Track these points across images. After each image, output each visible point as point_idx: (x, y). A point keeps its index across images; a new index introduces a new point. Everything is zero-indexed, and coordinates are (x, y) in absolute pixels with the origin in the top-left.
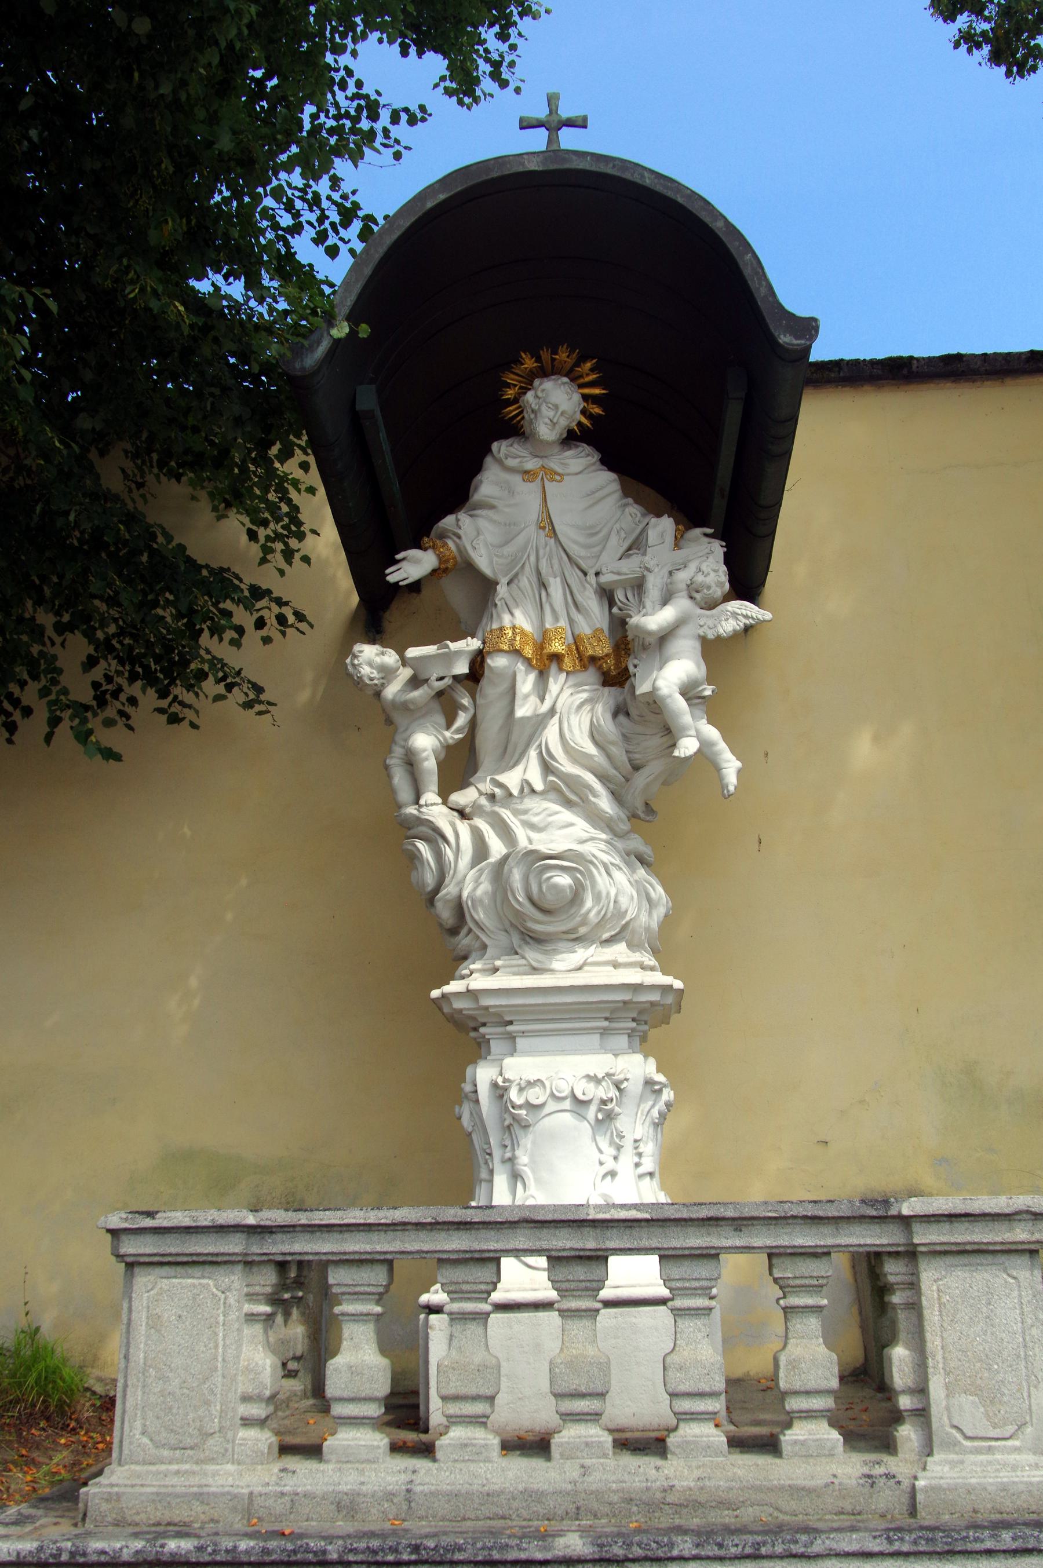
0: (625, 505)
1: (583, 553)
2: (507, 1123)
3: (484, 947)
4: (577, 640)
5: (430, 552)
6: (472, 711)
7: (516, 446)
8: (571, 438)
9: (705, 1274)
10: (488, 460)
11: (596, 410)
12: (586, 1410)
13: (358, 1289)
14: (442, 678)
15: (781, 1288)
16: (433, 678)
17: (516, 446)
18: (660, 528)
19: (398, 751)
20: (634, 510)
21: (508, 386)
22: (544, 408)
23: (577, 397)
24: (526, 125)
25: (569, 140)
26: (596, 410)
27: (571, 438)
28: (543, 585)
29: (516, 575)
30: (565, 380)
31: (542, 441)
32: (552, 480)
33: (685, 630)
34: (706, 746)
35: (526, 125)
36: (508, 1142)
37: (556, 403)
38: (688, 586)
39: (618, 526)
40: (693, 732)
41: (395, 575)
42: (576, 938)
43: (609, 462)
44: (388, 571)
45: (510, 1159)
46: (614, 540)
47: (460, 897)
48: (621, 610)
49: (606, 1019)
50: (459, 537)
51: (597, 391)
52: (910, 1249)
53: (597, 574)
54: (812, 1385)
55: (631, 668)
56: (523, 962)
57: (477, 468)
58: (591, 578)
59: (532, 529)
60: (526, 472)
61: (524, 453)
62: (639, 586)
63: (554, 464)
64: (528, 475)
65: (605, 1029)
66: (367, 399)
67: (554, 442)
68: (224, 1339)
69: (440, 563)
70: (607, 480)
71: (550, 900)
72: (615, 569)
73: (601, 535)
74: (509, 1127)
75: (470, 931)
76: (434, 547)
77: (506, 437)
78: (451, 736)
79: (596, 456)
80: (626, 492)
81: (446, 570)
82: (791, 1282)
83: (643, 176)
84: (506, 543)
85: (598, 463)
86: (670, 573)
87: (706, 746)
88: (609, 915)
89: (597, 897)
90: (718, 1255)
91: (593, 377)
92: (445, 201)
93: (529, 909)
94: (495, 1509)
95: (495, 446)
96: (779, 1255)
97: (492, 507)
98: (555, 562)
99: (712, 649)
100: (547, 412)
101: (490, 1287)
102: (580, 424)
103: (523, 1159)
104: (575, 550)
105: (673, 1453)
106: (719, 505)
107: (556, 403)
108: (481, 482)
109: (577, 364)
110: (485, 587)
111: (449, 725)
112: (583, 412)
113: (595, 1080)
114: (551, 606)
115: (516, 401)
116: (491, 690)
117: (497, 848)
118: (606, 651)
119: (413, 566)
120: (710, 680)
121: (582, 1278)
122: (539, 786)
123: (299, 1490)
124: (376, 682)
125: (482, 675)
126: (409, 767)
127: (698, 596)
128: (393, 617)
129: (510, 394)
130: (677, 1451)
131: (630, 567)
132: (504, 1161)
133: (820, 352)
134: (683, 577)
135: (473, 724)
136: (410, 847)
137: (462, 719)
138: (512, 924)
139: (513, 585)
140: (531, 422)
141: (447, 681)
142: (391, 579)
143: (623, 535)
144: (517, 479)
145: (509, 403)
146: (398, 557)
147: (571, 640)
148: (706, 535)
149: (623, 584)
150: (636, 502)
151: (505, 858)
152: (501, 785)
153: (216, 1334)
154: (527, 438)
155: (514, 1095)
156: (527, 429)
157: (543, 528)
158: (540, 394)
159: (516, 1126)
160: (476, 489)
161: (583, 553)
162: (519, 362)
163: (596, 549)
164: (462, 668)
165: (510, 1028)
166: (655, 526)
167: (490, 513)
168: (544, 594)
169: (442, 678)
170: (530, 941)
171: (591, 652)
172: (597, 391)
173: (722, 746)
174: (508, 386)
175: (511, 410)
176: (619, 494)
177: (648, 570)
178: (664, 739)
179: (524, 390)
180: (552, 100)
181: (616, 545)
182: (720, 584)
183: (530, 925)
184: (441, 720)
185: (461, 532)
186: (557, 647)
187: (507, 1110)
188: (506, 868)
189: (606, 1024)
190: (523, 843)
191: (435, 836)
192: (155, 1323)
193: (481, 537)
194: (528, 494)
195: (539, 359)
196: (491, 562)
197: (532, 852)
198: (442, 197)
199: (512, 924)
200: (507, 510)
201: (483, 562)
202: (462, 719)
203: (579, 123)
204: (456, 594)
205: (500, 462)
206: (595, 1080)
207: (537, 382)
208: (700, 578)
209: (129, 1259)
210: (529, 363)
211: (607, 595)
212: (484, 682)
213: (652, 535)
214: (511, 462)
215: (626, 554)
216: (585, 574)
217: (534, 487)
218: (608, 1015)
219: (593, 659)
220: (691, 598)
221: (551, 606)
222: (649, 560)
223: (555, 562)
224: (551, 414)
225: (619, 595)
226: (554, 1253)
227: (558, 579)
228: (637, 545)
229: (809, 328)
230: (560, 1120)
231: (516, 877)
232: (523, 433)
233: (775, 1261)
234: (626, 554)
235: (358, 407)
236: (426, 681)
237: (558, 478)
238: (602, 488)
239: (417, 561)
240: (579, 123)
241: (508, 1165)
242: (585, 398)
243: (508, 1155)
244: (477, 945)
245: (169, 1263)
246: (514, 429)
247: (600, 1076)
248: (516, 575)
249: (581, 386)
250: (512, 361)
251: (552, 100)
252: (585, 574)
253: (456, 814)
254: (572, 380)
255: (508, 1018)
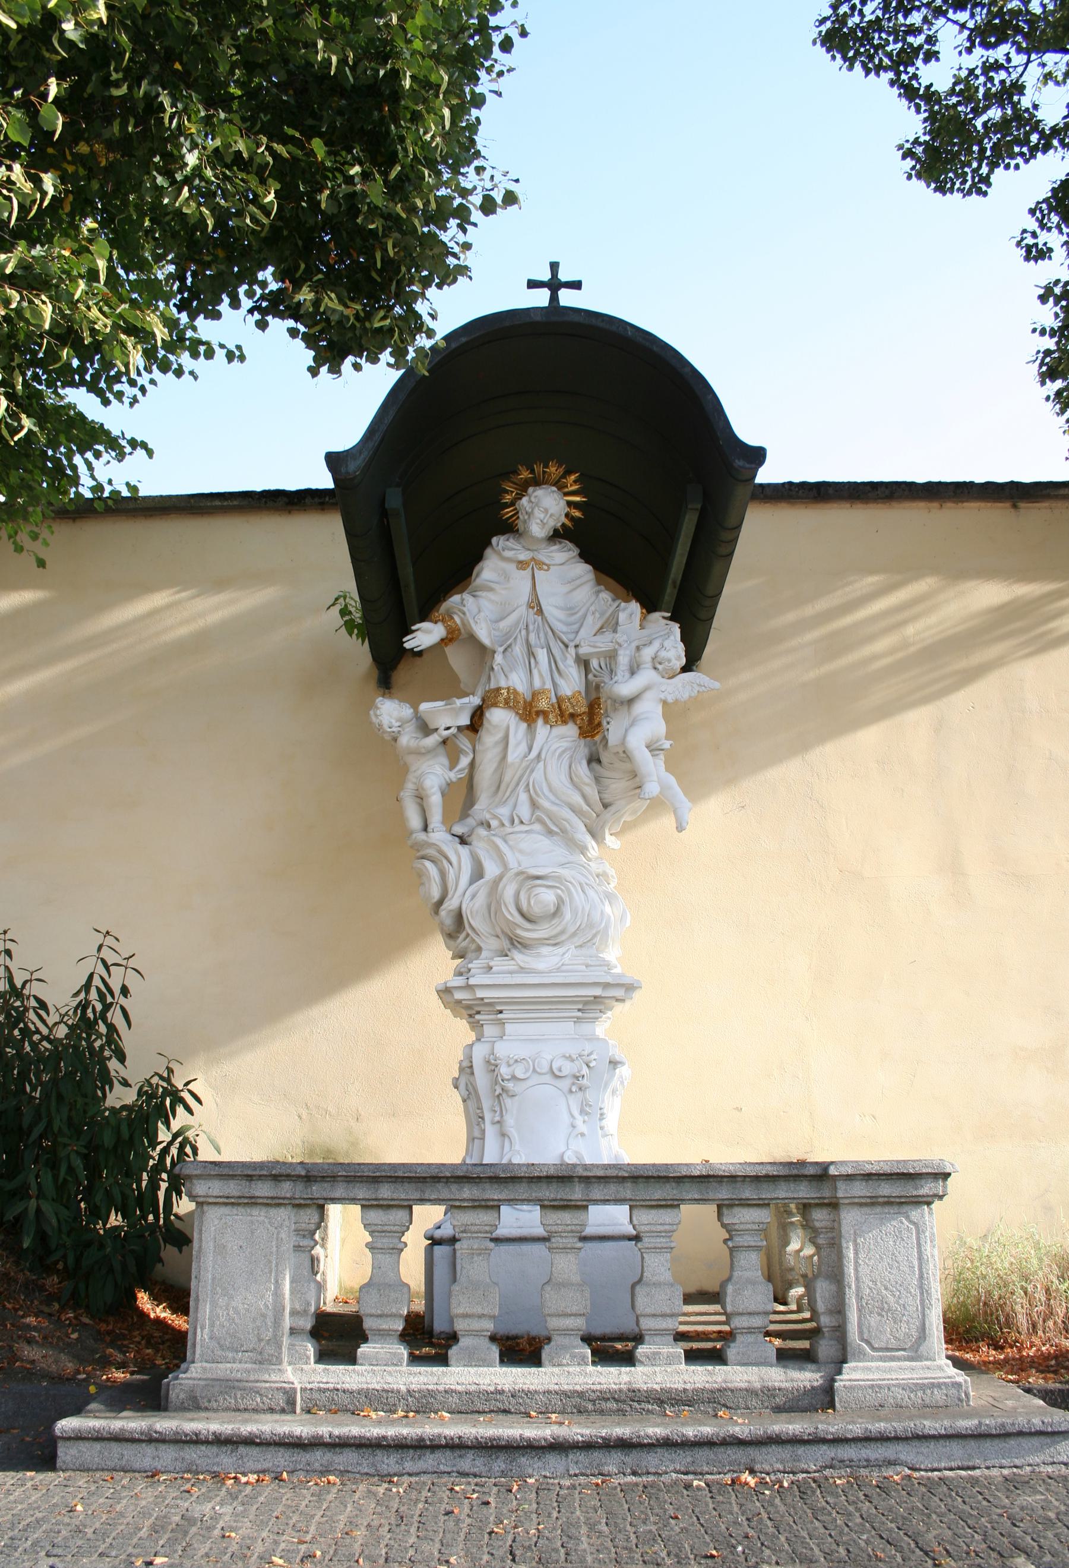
0: (599, 592)
1: (565, 629)
2: (497, 1093)
3: (479, 949)
4: (560, 700)
5: (440, 624)
6: (472, 756)
7: (511, 540)
8: (557, 535)
9: (668, 1220)
10: (488, 552)
11: (577, 514)
12: (571, 1326)
13: (386, 1228)
14: (448, 728)
15: (728, 1231)
16: (443, 728)
17: (511, 540)
18: (629, 611)
19: (410, 786)
20: (606, 596)
21: (507, 492)
22: (536, 510)
23: (563, 503)
24: (533, 284)
25: (567, 298)
26: (577, 514)
27: (557, 535)
28: (531, 654)
29: (509, 646)
30: (554, 488)
31: (532, 537)
32: (540, 569)
33: (648, 695)
34: (664, 787)
35: (533, 284)
36: (497, 1109)
37: (546, 507)
38: (653, 659)
39: (592, 608)
40: (655, 778)
41: (412, 642)
42: (554, 941)
43: (585, 556)
44: (404, 640)
45: (498, 1122)
46: (590, 619)
47: (460, 908)
48: (595, 676)
49: (579, 1010)
50: (464, 614)
51: (577, 499)
52: (834, 1200)
53: (576, 646)
54: (752, 1308)
55: (604, 723)
56: (512, 962)
57: (479, 558)
58: (572, 650)
59: (523, 610)
60: (521, 562)
61: (518, 547)
62: (611, 656)
63: (542, 557)
64: (522, 565)
65: (578, 1018)
66: (394, 500)
67: (542, 539)
68: (277, 1266)
69: (448, 633)
70: (583, 570)
71: (537, 910)
72: (591, 644)
73: (578, 615)
74: (498, 1096)
75: (468, 935)
76: (443, 621)
77: (503, 533)
78: (453, 776)
79: (575, 551)
80: (599, 582)
81: (451, 640)
82: (737, 1227)
83: (626, 329)
84: (502, 619)
85: (578, 559)
86: (638, 648)
87: (664, 787)
88: (583, 926)
89: (575, 913)
90: (678, 1205)
91: (575, 487)
92: (467, 343)
93: (519, 919)
94: (500, 1405)
95: (494, 540)
96: (731, 1206)
97: (491, 589)
98: (542, 635)
99: (671, 711)
100: (538, 514)
101: (405, 1228)
102: (563, 525)
103: (510, 1121)
104: (558, 626)
105: (642, 1362)
106: (670, 594)
107: (546, 507)
108: (482, 569)
109: (564, 476)
110: (482, 653)
111: (451, 769)
112: (567, 515)
113: (570, 1059)
114: (540, 672)
115: (512, 504)
116: (489, 739)
117: (491, 870)
118: (583, 709)
119: (425, 636)
120: (668, 737)
121: (569, 1222)
122: (526, 817)
123: (339, 1387)
124: (394, 729)
125: (482, 724)
126: (419, 800)
127: (660, 667)
128: (401, 675)
129: (508, 498)
130: (643, 1359)
131: (604, 643)
132: (493, 1123)
133: (765, 475)
134: (648, 653)
135: (472, 765)
136: (419, 866)
137: (464, 762)
138: (503, 932)
139: (507, 653)
140: (525, 522)
141: (453, 730)
142: (407, 646)
143: (597, 615)
144: (511, 567)
145: (507, 505)
146: (413, 628)
147: (554, 700)
148: (664, 618)
149: (598, 655)
150: (607, 589)
151: (500, 878)
152: (495, 817)
153: (270, 1262)
154: (521, 535)
155: (504, 1070)
156: (521, 526)
157: (533, 608)
158: (533, 499)
159: (504, 1095)
160: (478, 575)
161: (565, 629)
162: (516, 472)
163: (576, 627)
164: (465, 720)
165: (500, 1016)
166: (624, 610)
167: (490, 595)
168: (532, 661)
169: (448, 728)
170: (519, 946)
171: (571, 711)
172: (577, 499)
173: (678, 789)
174: (507, 492)
175: (508, 512)
176: (593, 583)
177: (620, 645)
178: (630, 783)
179: (519, 497)
180: (554, 266)
181: (591, 623)
182: (678, 658)
183: (519, 932)
184: (445, 761)
185: (465, 609)
186: (543, 705)
187: (496, 1082)
188: (501, 885)
189: (580, 1014)
190: (512, 864)
191: (439, 858)
192: (221, 1249)
193: (482, 614)
194: (521, 582)
195: (532, 471)
196: (490, 634)
197: (522, 873)
198: (464, 340)
199: (503, 932)
200: (503, 592)
201: (483, 634)
202: (464, 762)
203: (576, 285)
204: (457, 658)
205: (499, 554)
206: (570, 1059)
207: (531, 489)
208: (663, 654)
209: (201, 1200)
210: (525, 474)
211: (584, 663)
212: (483, 733)
213: (622, 617)
214: (508, 554)
215: (600, 631)
216: (567, 646)
217: (527, 573)
218: (580, 1007)
219: (573, 716)
220: (655, 668)
221: (540, 672)
222: (620, 637)
223: (542, 635)
224: (542, 516)
225: (594, 663)
226: (546, 1203)
227: (545, 650)
228: (611, 625)
229: (758, 455)
230: (546, 1091)
231: (508, 892)
232: (518, 530)
233: (725, 1211)
234: (600, 631)
235: (386, 506)
236: (437, 729)
237: (545, 567)
238: (581, 577)
239: (428, 632)
240: (576, 285)
241: (497, 1126)
242: (569, 504)
243: (497, 1119)
244: (473, 947)
245: (233, 1204)
246: (509, 528)
247: (574, 1057)
248: (509, 646)
249: (566, 494)
250: (510, 473)
251: (554, 266)
252: (567, 646)
253: (457, 839)
254: (559, 489)
255: (499, 1008)
